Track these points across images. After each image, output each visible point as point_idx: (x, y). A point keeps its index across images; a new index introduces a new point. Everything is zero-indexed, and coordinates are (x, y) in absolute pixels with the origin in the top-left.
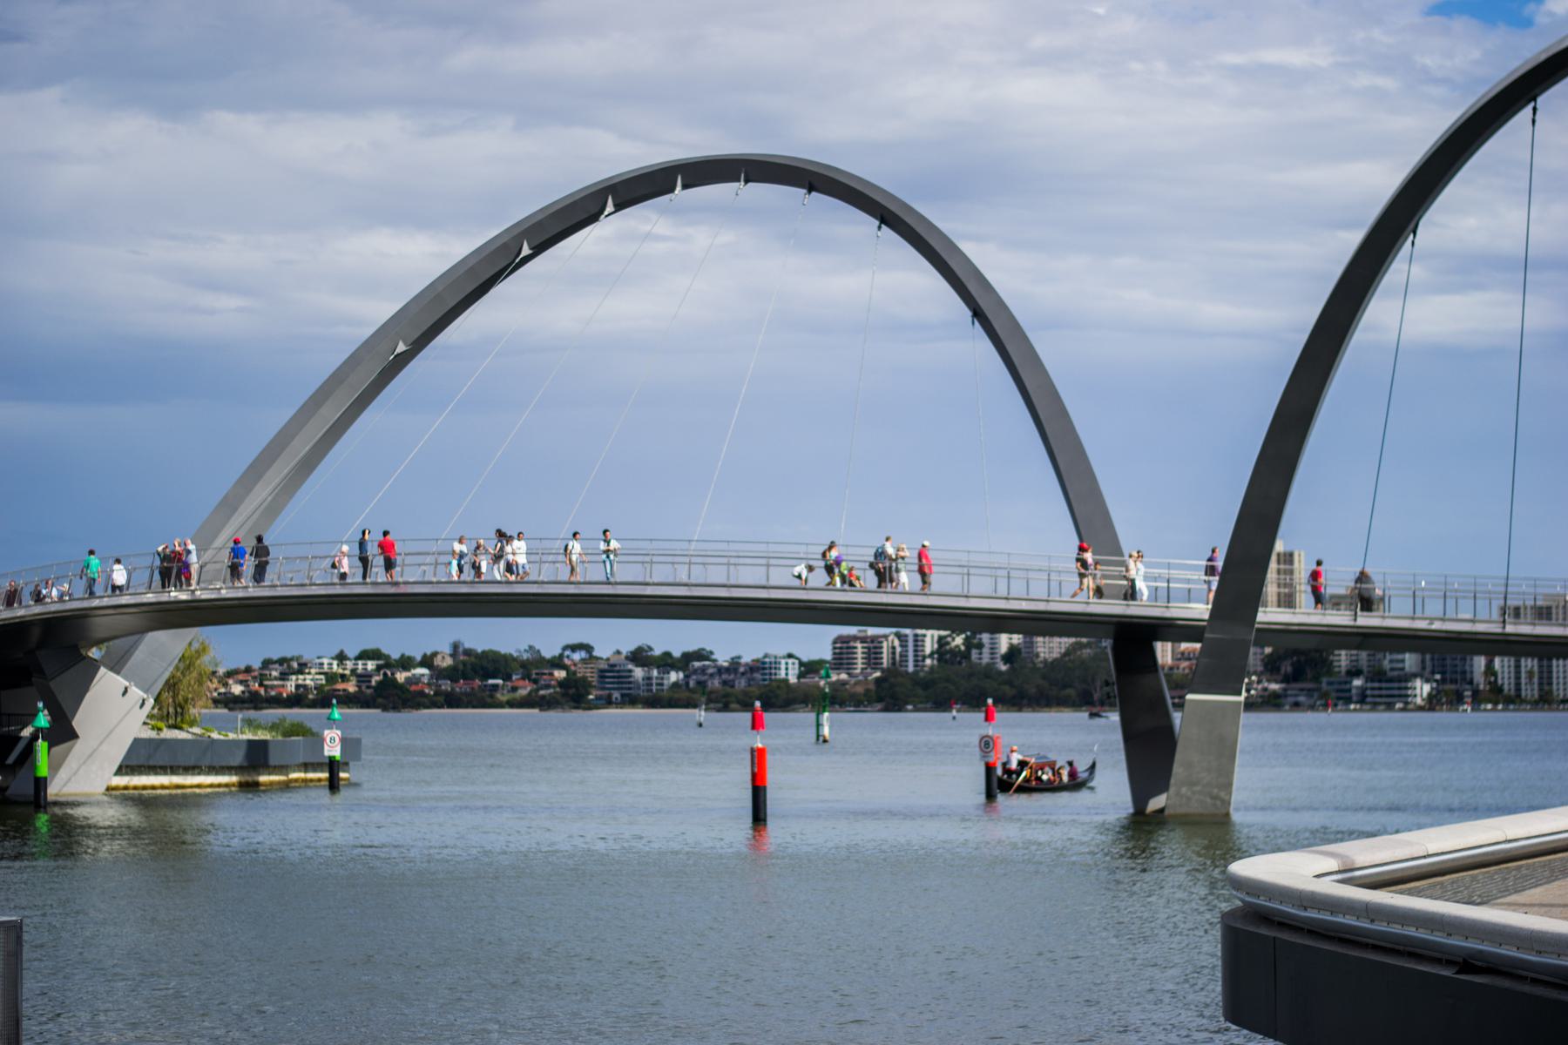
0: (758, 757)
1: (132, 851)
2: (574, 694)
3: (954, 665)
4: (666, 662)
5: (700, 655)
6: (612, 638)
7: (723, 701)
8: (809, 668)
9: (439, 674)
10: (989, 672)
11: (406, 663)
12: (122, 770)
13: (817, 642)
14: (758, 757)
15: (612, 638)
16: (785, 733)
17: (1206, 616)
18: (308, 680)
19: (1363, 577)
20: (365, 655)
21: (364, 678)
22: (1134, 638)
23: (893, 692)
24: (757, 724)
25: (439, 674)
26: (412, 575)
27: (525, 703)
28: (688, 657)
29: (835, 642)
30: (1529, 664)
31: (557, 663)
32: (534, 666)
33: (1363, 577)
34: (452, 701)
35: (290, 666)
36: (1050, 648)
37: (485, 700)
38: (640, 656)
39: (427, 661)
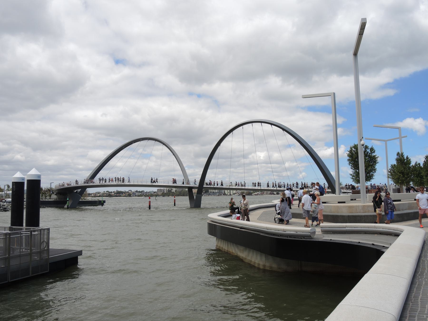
1: (250, 295)
2: (130, 195)
4: (139, 192)
5: (143, 191)
6: (134, 189)
7: (146, 196)
8: (155, 192)
9: (115, 193)
10: (173, 193)
11: (111, 192)
12: (104, 202)
14: (150, 202)
15: (134, 189)
17: (41, 210)
21: (107, 194)
22: (190, 189)
23: (164, 195)
24: (150, 198)
25: (115, 193)
27: (125, 196)
28: (142, 191)
29: (374, 151)
30: (228, 191)
31: (128, 192)
32: (125, 192)
35: (99, 193)
38: (137, 191)
39: (114, 192)
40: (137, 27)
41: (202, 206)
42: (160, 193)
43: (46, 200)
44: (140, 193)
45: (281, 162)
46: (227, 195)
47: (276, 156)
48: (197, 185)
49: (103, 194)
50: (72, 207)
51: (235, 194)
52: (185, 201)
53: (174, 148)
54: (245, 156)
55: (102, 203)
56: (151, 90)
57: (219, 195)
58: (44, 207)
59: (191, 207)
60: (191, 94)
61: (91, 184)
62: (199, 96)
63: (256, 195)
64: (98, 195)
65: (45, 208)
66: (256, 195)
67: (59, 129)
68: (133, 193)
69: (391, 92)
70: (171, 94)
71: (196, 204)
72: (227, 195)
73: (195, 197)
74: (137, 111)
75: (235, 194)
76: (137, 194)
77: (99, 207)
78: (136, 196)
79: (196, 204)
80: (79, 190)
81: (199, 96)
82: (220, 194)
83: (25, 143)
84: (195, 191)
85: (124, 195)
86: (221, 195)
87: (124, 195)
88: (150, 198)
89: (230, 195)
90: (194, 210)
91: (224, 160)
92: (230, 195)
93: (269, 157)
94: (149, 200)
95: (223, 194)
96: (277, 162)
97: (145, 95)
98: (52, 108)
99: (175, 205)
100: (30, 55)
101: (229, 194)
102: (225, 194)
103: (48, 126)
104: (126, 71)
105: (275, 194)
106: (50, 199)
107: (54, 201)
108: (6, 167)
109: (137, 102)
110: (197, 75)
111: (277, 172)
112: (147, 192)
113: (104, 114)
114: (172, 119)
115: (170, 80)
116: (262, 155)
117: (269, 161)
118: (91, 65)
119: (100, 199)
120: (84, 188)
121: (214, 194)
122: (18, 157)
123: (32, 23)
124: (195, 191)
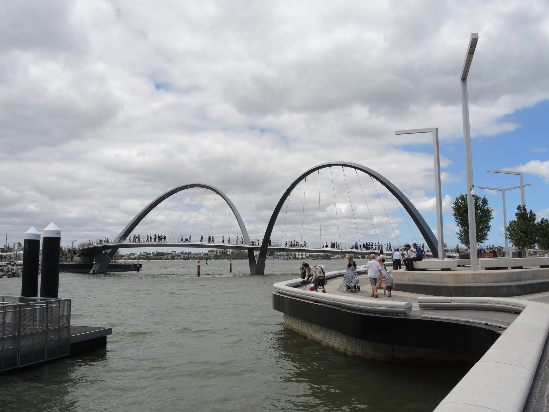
0: (231, 264)
2: (173, 258)
3: (225, 253)
4: (186, 253)
5: (190, 253)
8: (205, 254)
9: (154, 255)
11: (150, 254)
12: (141, 266)
13: (206, 251)
14: (231, 264)
15: (178, 250)
16: (202, 263)
18: (136, 256)
19: (531, 211)
20: (144, 253)
21: (144, 256)
23: (217, 257)
24: (199, 262)
25: (154, 255)
26: (168, 242)
30: (300, 253)
31: (171, 254)
32: (167, 254)
33: (531, 211)
34: (156, 259)
35: (134, 254)
36: (230, 251)
37: (161, 259)
38: (182, 253)
39: (153, 253)
40: (184, 41)
41: (266, 272)
42: (212, 255)
43: (67, 263)
46: (298, 258)
47: (361, 208)
49: (139, 256)
51: (308, 257)
54: (321, 209)
57: (287, 259)
60: (252, 128)
62: (263, 130)
63: (335, 259)
64: (133, 257)
66: (335, 259)
67: (83, 172)
68: (178, 255)
69: (511, 127)
70: (226, 128)
71: (258, 270)
72: (298, 258)
74: (182, 149)
75: (308, 257)
76: (183, 256)
78: (181, 259)
79: (258, 270)
80: (109, 251)
81: (263, 130)
82: (289, 258)
83: (41, 190)
84: (256, 253)
88: (199, 262)
89: (302, 258)
91: (294, 214)
93: (353, 210)
95: (293, 258)
97: (193, 129)
98: (75, 145)
99: (231, 271)
100: (46, 76)
101: (300, 257)
102: (295, 258)
103: (69, 168)
104: (169, 98)
105: (359, 258)
106: (71, 261)
108: (16, 220)
109: (183, 139)
112: (195, 254)
113: (142, 154)
114: (228, 160)
115: (225, 110)
116: (343, 207)
117: (352, 215)
118: (124, 89)
119: (136, 262)
120: (115, 248)
121: (281, 257)
122: (32, 207)
123: (48, 34)
124: (256, 253)
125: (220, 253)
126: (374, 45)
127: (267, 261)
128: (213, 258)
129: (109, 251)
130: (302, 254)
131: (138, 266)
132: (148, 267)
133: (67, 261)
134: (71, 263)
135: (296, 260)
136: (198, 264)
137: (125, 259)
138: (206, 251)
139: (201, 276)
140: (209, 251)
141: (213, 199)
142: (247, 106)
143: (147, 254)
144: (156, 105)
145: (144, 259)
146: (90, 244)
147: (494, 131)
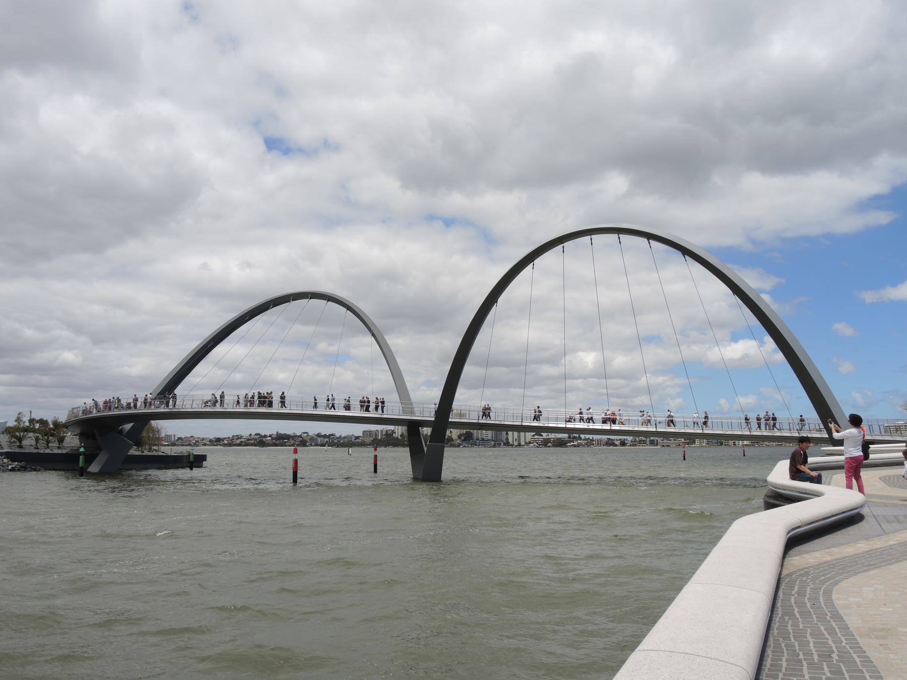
4: (325, 436)
5: (332, 435)
8: (357, 438)
9: (273, 439)
11: (266, 436)
13: (357, 430)
14: (296, 461)
20: (256, 434)
21: (255, 440)
22: (414, 426)
24: (296, 451)
25: (273, 439)
30: (516, 434)
31: (300, 436)
34: (276, 445)
39: (270, 436)
40: (307, 60)
41: (446, 474)
42: (368, 440)
43: (48, 451)
44: (327, 440)
45: (628, 375)
46: (512, 445)
47: (620, 361)
48: (429, 415)
49: (249, 440)
50: (105, 474)
51: (530, 443)
52: (398, 461)
53: (394, 341)
54: (553, 361)
55: (197, 461)
56: (341, 211)
57: (494, 446)
58: (35, 470)
59: (415, 479)
60: (431, 218)
61: (163, 409)
62: (449, 222)
63: (575, 446)
64: (238, 442)
65: (39, 470)
66: (575, 446)
67: (148, 299)
68: (312, 439)
69: (882, 218)
70: (384, 216)
71: (428, 470)
72: (512, 445)
73: (425, 449)
74: (314, 256)
75: (530, 443)
76: (319, 440)
77: (184, 473)
78: (317, 445)
79: (428, 470)
80: (128, 426)
81: (449, 222)
82: (497, 443)
83: (77, 328)
84: (426, 431)
85: (292, 442)
86: (499, 445)
87: (292, 442)
88: (296, 451)
89: (520, 445)
90: (423, 488)
91: (504, 369)
92: (520, 445)
93: (605, 364)
94: (294, 456)
95: (505, 444)
96: (619, 375)
97: (329, 223)
98: (132, 249)
99: (375, 471)
100: (70, 122)
101: (516, 443)
102: (507, 444)
103: (123, 290)
104: (290, 169)
105: (616, 445)
106: (59, 448)
107: (66, 454)
108: (46, 379)
109: (315, 239)
110: (439, 170)
111: (618, 396)
112: (340, 437)
113: (248, 265)
114: (391, 276)
115: (384, 186)
116: (589, 359)
117: (603, 373)
118: (209, 149)
119: (198, 451)
120: (142, 420)
121: (483, 442)
122: (69, 357)
123: (72, 50)
124: (426, 431)
125: (382, 435)
126: (648, 61)
127: (448, 452)
128: (370, 444)
129: (128, 426)
130: (519, 437)
131: (192, 459)
132: (216, 458)
133: (48, 447)
134: (60, 451)
135: (510, 448)
136: (294, 456)
137: (225, 445)
138: (357, 430)
139: (299, 485)
140: (364, 432)
141: (366, 345)
142: (420, 177)
143: (261, 436)
144: (269, 179)
145: (256, 445)
146: (85, 412)
147: (851, 224)
